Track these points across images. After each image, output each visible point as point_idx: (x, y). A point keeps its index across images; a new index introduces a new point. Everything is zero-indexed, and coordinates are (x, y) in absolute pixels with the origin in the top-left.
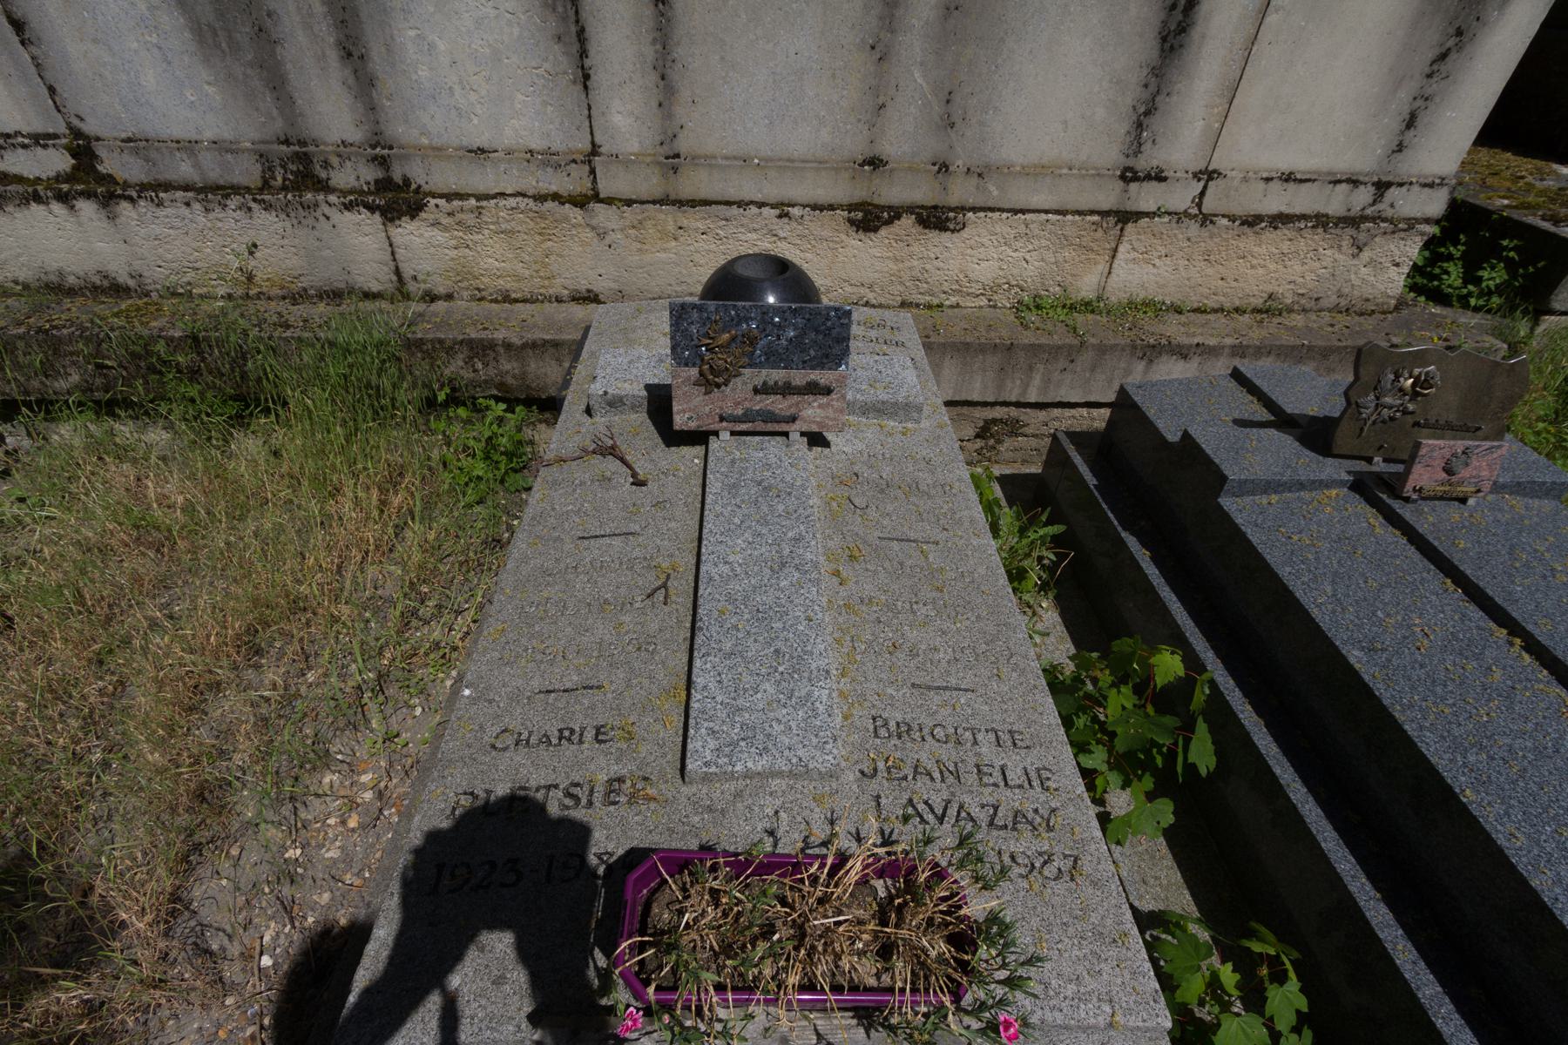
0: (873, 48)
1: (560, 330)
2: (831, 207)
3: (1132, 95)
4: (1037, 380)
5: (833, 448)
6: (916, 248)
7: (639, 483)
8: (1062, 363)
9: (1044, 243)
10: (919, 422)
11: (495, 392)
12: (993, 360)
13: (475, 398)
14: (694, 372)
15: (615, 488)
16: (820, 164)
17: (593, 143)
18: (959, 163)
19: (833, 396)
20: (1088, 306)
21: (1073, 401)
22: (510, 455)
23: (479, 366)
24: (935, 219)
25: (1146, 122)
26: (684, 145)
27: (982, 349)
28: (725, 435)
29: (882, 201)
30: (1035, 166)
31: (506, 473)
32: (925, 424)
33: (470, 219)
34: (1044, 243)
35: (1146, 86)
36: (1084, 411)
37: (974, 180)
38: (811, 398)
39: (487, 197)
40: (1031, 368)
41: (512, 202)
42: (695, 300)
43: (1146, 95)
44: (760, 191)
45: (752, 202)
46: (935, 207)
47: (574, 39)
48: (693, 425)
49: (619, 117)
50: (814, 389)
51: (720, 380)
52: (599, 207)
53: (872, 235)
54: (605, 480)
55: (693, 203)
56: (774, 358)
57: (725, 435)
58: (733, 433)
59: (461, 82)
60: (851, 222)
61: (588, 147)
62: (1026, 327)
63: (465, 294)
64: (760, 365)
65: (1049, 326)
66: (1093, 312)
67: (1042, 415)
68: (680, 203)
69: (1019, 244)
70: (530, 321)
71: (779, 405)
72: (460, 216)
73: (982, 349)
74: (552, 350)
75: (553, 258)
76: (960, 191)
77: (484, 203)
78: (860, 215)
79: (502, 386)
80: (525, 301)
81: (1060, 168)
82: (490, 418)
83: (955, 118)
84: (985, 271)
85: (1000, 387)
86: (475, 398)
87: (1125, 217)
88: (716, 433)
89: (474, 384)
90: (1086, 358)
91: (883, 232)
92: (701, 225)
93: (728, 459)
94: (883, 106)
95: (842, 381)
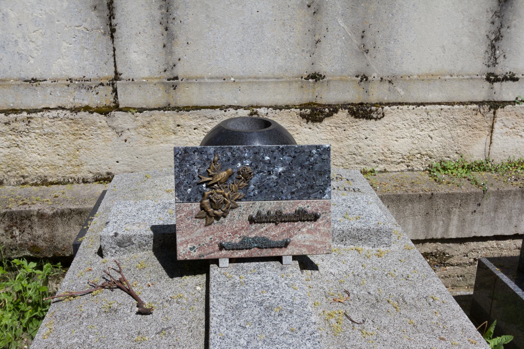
0: (309, 6)
1: (84, 202)
2: (288, 107)
3: (485, 28)
4: (455, 220)
5: (321, 270)
6: (350, 132)
7: (144, 312)
8: (472, 207)
9: (441, 124)
10: (388, 245)
11: (28, 253)
12: (420, 207)
13: (11, 259)
14: (196, 206)
15: (120, 318)
16: (278, 79)
17: (116, 73)
18: (375, 75)
19: (320, 221)
20: (480, 167)
21: (484, 235)
22: (35, 305)
23: (17, 232)
24: (362, 111)
25: (497, 44)
26: (180, 71)
27: (410, 199)
28: (224, 262)
29: (323, 102)
30: (427, 75)
31: (30, 320)
32: (394, 247)
33: (21, 126)
34: (441, 124)
35: (493, 23)
36: (494, 243)
37: (387, 85)
38: (300, 224)
39: (36, 111)
40: (449, 212)
41: (54, 113)
42: (198, 145)
43: (494, 28)
44: (235, 98)
45: (230, 106)
46: (362, 104)
47: (106, 7)
48: (195, 255)
49: (135, 55)
50: (302, 216)
51: (219, 212)
52: (118, 114)
53: (318, 124)
54: (111, 311)
55: (188, 109)
56: (266, 191)
57: (224, 262)
58: (232, 260)
59: (24, 37)
60: (303, 116)
61: (113, 75)
62: (440, 182)
63: (13, 181)
64: (254, 198)
65: (456, 181)
66: (484, 170)
67: (462, 248)
68: (178, 109)
69: (424, 126)
70: (61, 197)
71: (272, 232)
72: (13, 125)
73: (410, 199)
74: (76, 217)
75: (82, 151)
76: (377, 93)
77: (33, 115)
78: (309, 111)
79: (34, 248)
80: (58, 183)
81: (444, 75)
82: (21, 273)
83: (368, 47)
84: (403, 146)
85: (428, 228)
86: (11, 259)
87: (495, 105)
88: (216, 261)
89: (12, 248)
90: (488, 203)
91: (326, 121)
92: (194, 123)
93: (229, 284)
94: (318, 41)
95: (327, 208)
